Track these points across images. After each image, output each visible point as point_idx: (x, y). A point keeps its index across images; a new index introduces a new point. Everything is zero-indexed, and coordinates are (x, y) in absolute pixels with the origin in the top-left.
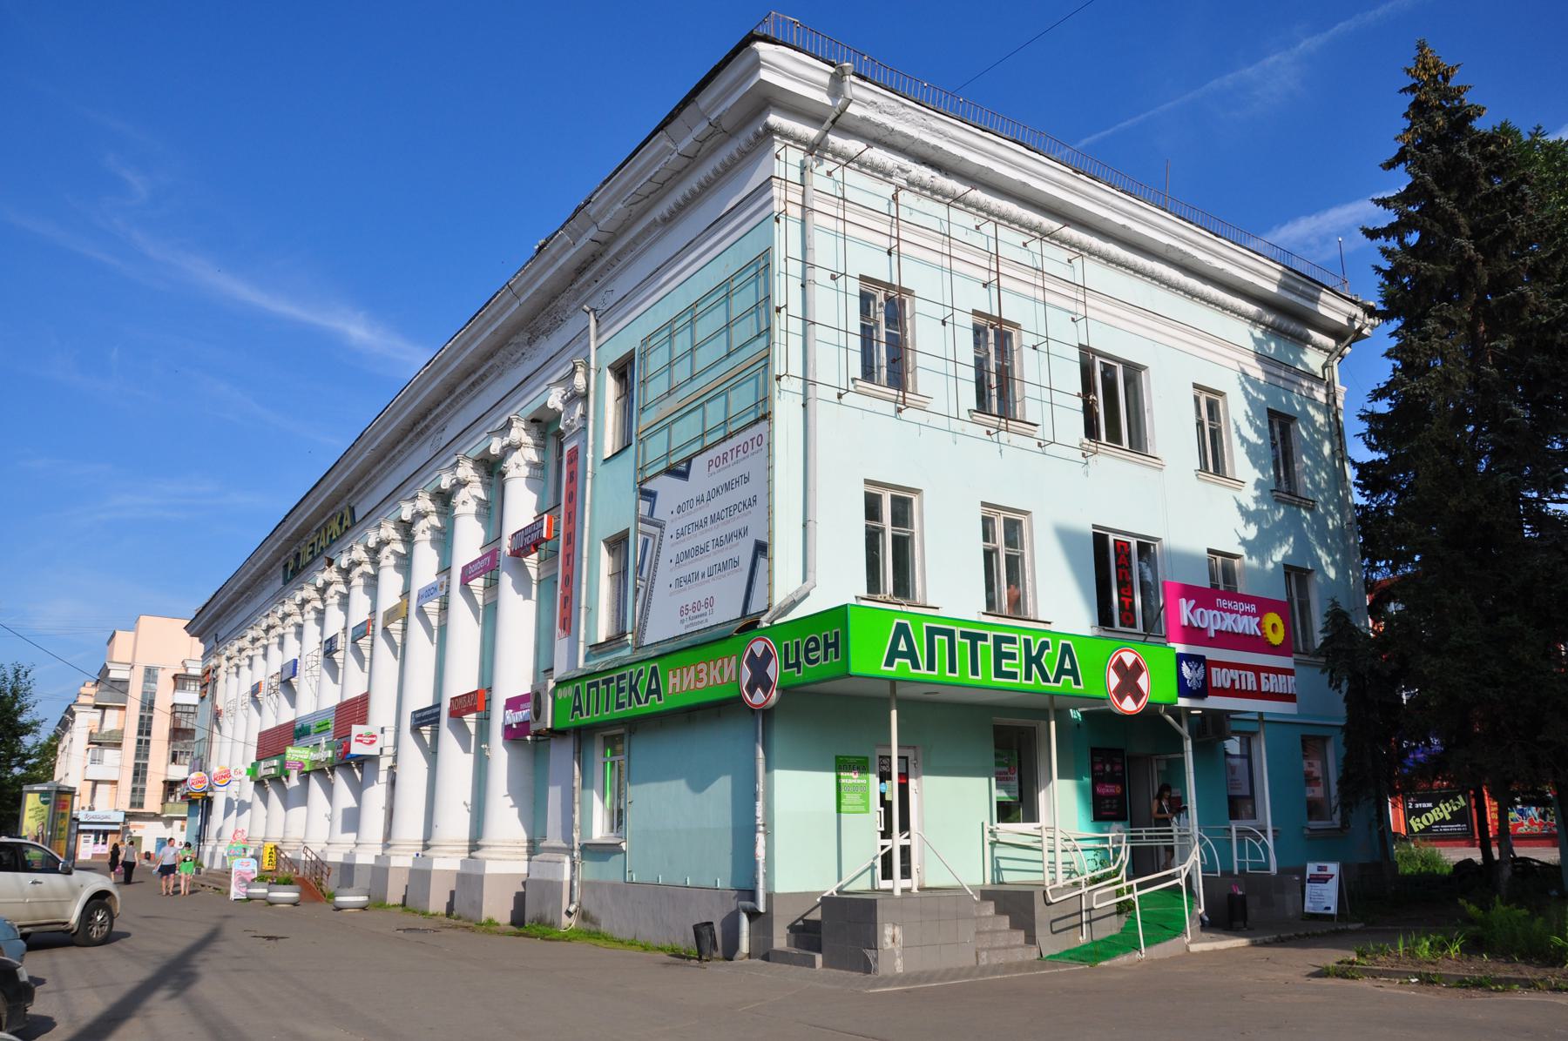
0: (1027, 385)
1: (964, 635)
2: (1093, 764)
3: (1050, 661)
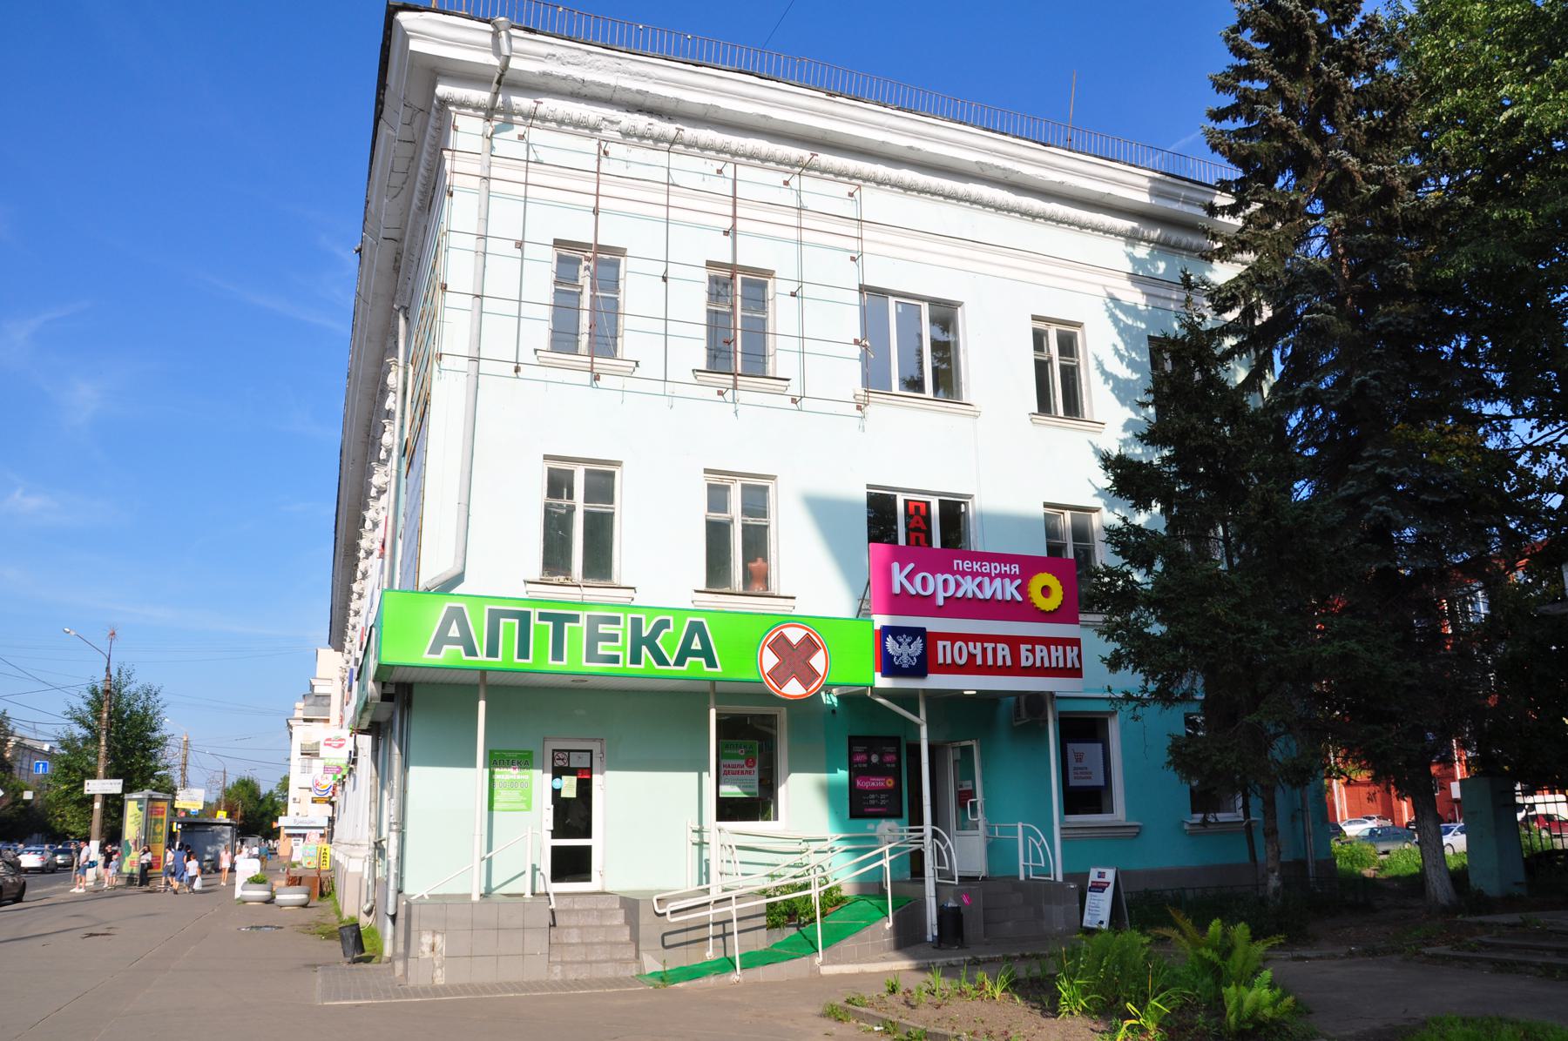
1: (543, 617)
3: (670, 643)
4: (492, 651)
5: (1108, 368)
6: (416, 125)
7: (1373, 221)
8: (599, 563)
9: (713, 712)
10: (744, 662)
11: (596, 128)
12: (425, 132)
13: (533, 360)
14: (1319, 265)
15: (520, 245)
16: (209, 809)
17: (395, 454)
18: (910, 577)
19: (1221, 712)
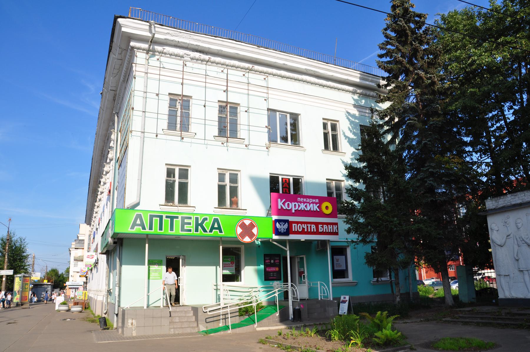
0: (251, 125)
1: (167, 217)
2: (265, 260)
3: (207, 225)
4: (151, 228)
5: (346, 135)
6: (123, 54)
7: (428, 90)
8: (183, 199)
9: (221, 247)
10: (231, 231)
11: (182, 57)
12: (126, 56)
13: (162, 133)
14: (413, 105)
15: (157, 95)
16: (42, 280)
17: (114, 161)
18: (284, 204)
19: (382, 245)
